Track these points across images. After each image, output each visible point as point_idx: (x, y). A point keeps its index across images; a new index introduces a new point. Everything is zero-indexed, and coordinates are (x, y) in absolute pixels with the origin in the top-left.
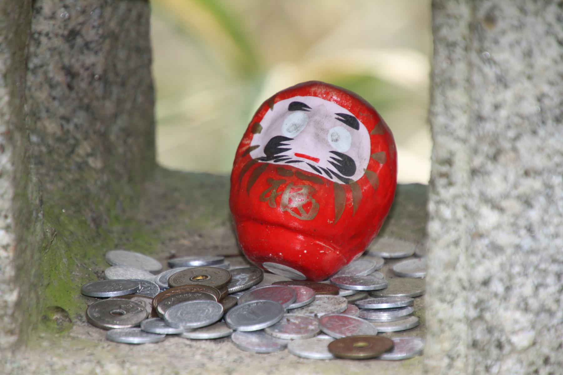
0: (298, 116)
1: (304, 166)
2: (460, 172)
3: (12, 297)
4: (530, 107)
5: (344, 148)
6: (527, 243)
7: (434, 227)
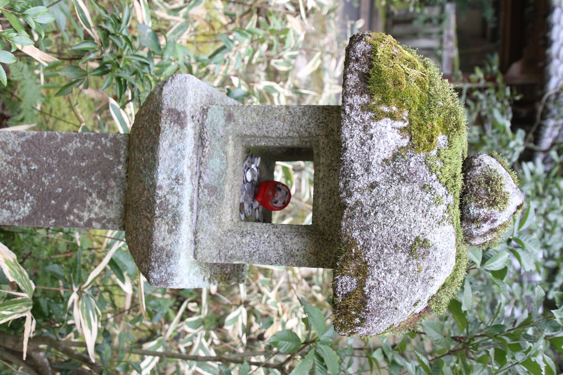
0: (285, 193)
1: (276, 195)
2: (274, 230)
3: (252, 145)
4: (286, 243)
5: (279, 202)
6: (261, 242)
7: (264, 224)
